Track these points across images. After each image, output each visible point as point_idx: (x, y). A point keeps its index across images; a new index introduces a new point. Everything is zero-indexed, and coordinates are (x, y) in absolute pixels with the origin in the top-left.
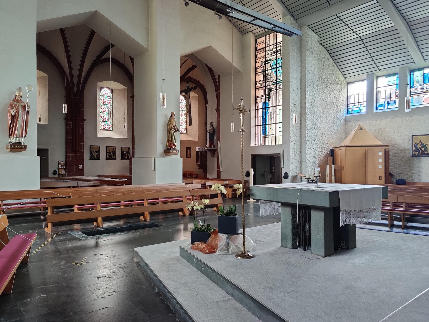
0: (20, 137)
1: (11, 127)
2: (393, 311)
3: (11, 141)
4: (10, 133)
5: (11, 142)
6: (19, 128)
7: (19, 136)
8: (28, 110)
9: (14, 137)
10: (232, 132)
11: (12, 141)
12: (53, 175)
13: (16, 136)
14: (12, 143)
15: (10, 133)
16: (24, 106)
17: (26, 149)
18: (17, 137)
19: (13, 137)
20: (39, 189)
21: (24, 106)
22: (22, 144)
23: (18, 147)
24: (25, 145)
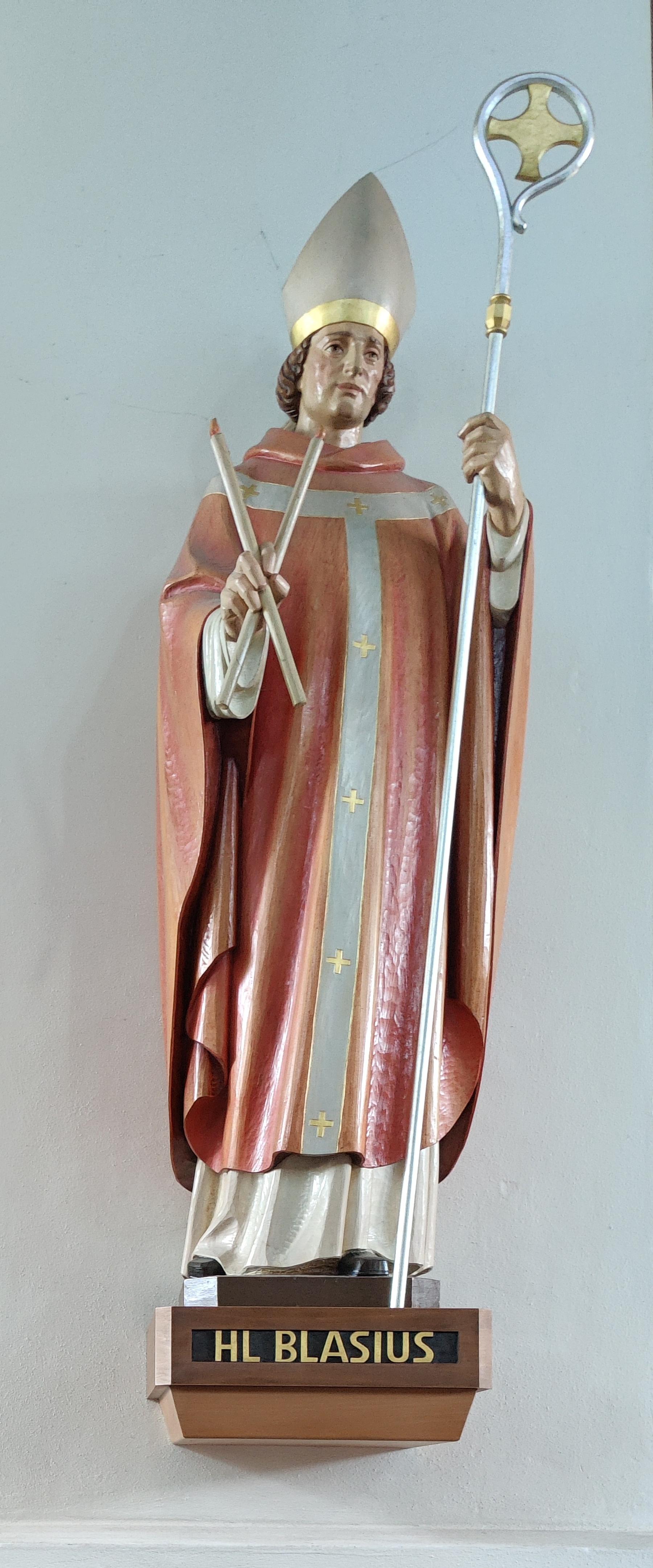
0: (356, 1160)
1: (206, 959)
2: (302, 1278)
3: (206, 1249)
4: (195, 1091)
5: (210, 1268)
6: (338, 963)
7: (347, 1135)
8: (500, 599)
9: (260, 1156)
10: (397, 1310)
11: (227, 1240)
12: (427, 1353)
13: (294, 1135)
14: (212, 1282)
15: (195, 1091)
16: (430, 532)
17: (471, 1388)
18: (305, 1148)
19: (245, 1174)
20: (333, 1152)
21: (430, 532)
22: (397, 1299)
23: (315, 1350)
24: (445, 1303)
